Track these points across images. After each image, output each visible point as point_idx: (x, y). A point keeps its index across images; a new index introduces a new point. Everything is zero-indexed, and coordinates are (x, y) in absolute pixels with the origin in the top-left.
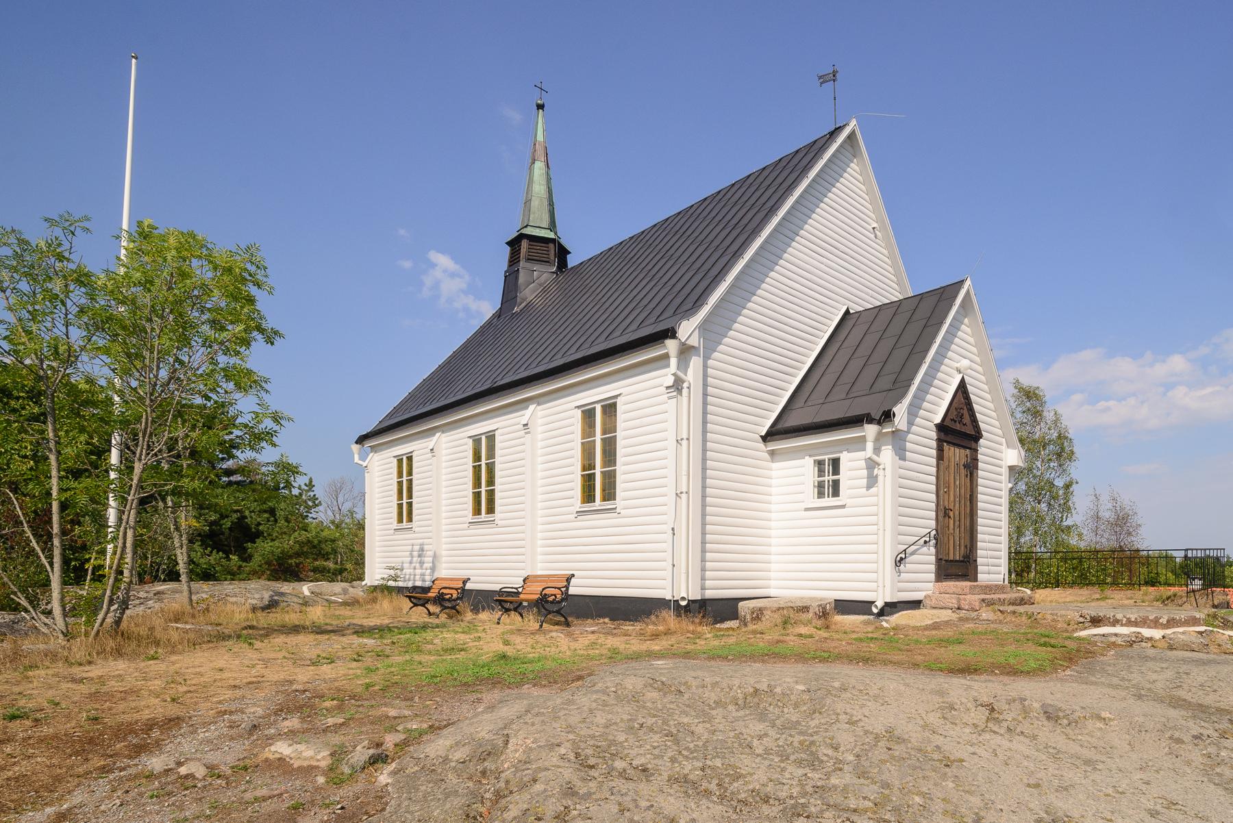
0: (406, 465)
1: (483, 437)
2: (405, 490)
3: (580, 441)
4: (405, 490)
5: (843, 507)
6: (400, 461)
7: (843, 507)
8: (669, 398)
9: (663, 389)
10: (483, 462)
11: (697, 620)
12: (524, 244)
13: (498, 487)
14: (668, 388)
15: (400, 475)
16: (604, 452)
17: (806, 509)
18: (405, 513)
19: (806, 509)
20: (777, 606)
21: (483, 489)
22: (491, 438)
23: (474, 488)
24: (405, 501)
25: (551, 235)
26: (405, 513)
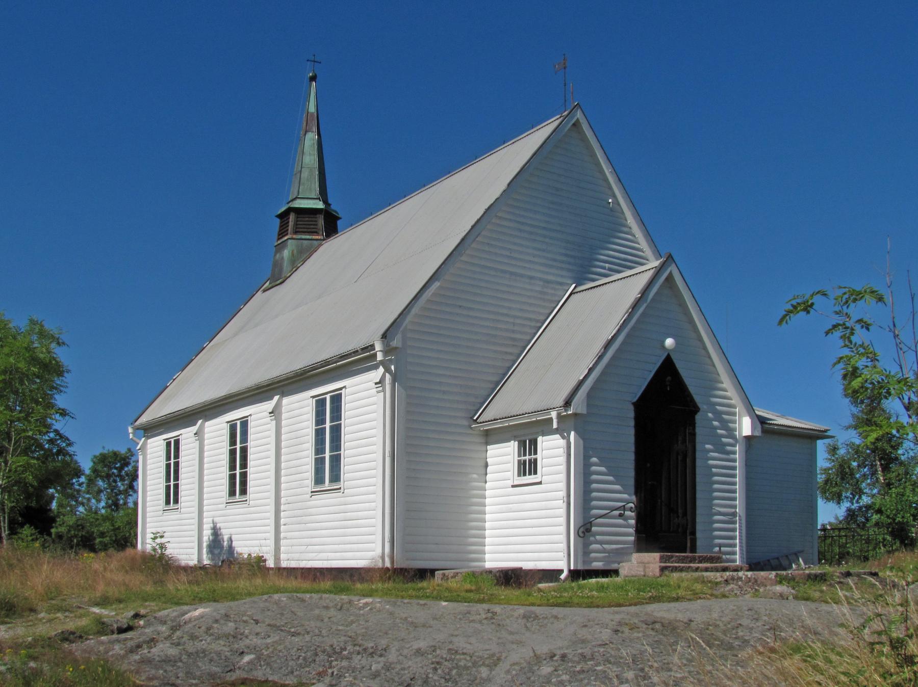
0: (173, 449)
1: (238, 422)
2: (173, 472)
3: (314, 428)
4: (173, 472)
5: (540, 483)
6: (169, 444)
7: (540, 483)
8: (378, 392)
9: (372, 385)
10: (238, 446)
11: (72, 556)
12: (292, 217)
13: (250, 470)
14: (376, 384)
15: (168, 458)
16: (332, 441)
17: (513, 486)
18: (172, 496)
19: (513, 486)
20: (808, 603)
21: (238, 471)
22: (245, 424)
23: (317, 423)
24: (172, 483)
25: (320, 205)
26: (172, 496)
